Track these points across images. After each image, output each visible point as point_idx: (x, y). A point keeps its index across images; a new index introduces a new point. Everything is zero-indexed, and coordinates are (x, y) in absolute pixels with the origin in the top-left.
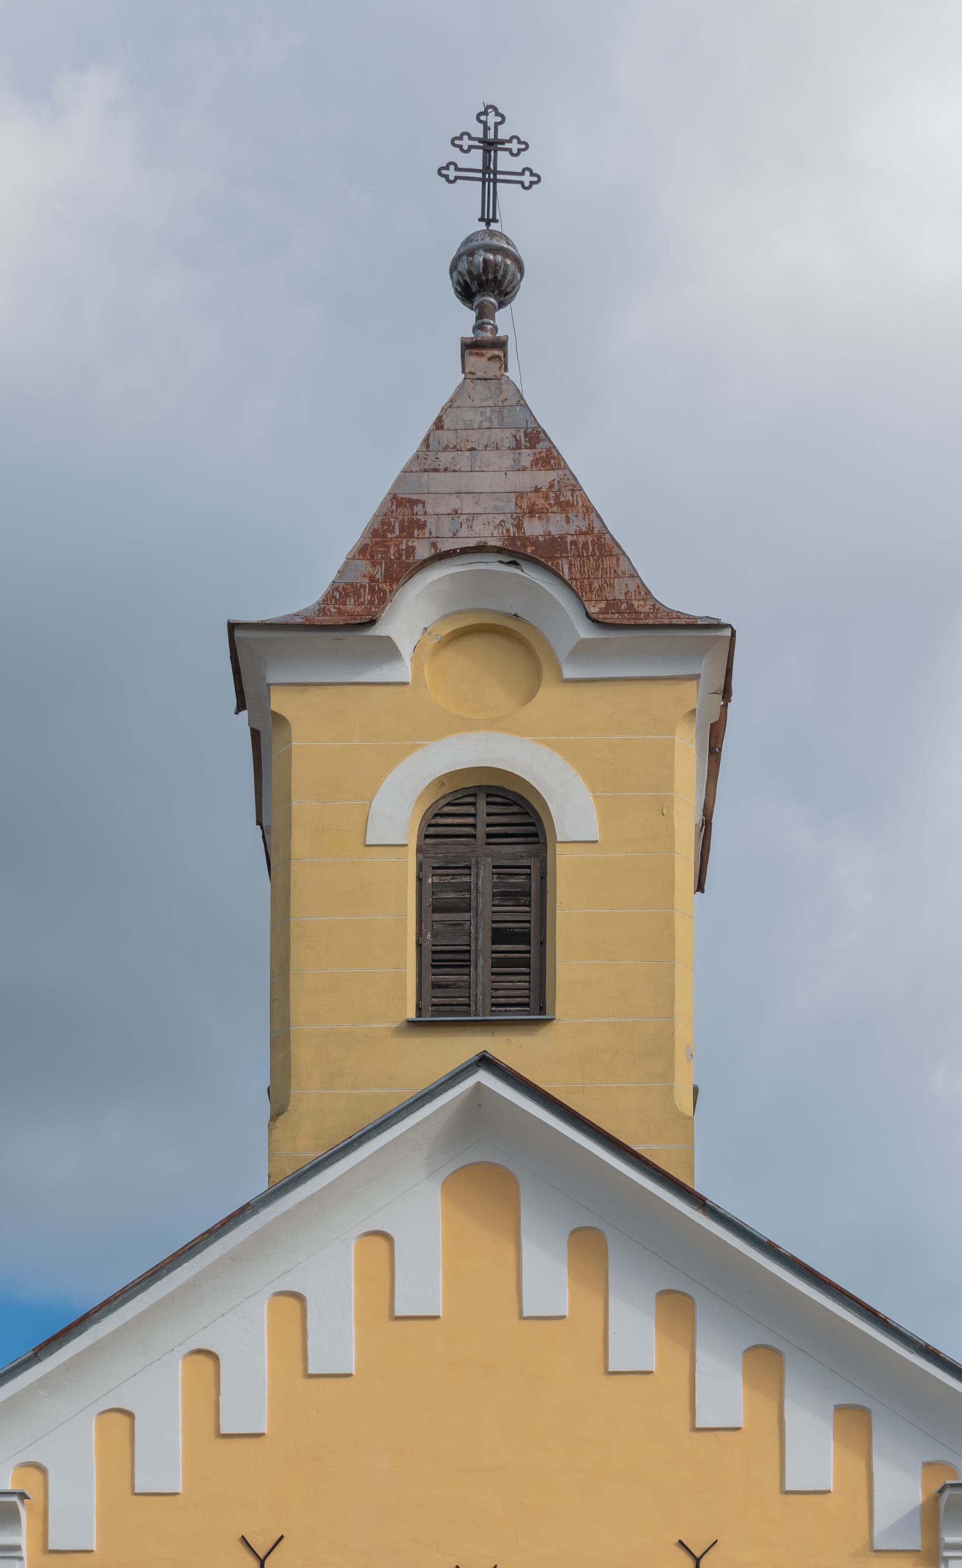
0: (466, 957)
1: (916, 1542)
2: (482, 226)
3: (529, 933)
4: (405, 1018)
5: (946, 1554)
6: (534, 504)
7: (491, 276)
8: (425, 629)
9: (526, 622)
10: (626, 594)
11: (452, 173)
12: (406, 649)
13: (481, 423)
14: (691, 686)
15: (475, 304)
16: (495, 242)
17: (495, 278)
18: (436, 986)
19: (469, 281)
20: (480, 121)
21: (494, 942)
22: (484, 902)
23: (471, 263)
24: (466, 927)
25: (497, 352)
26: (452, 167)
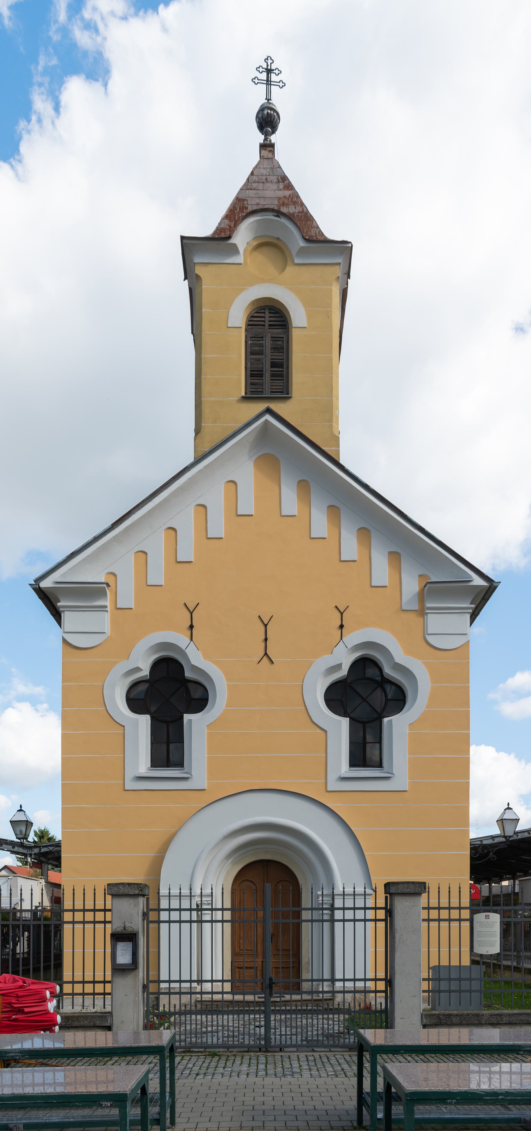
0: (262, 373)
1: (416, 607)
2: (267, 101)
3: (283, 364)
4: (241, 396)
5: (427, 611)
6: (284, 202)
7: (269, 119)
8: (248, 243)
9: (282, 241)
10: (315, 234)
11: (256, 81)
12: (241, 249)
13: (266, 173)
14: (337, 267)
15: (264, 131)
16: (271, 106)
17: (271, 120)
18: (252, 384)
19: (262, 121)
20: (265, 62)
21: (272, 367)
22: (268, 351)
23: (263, 114)
24: (262, 360)
25: (271, 149)
26: (256, 79)
